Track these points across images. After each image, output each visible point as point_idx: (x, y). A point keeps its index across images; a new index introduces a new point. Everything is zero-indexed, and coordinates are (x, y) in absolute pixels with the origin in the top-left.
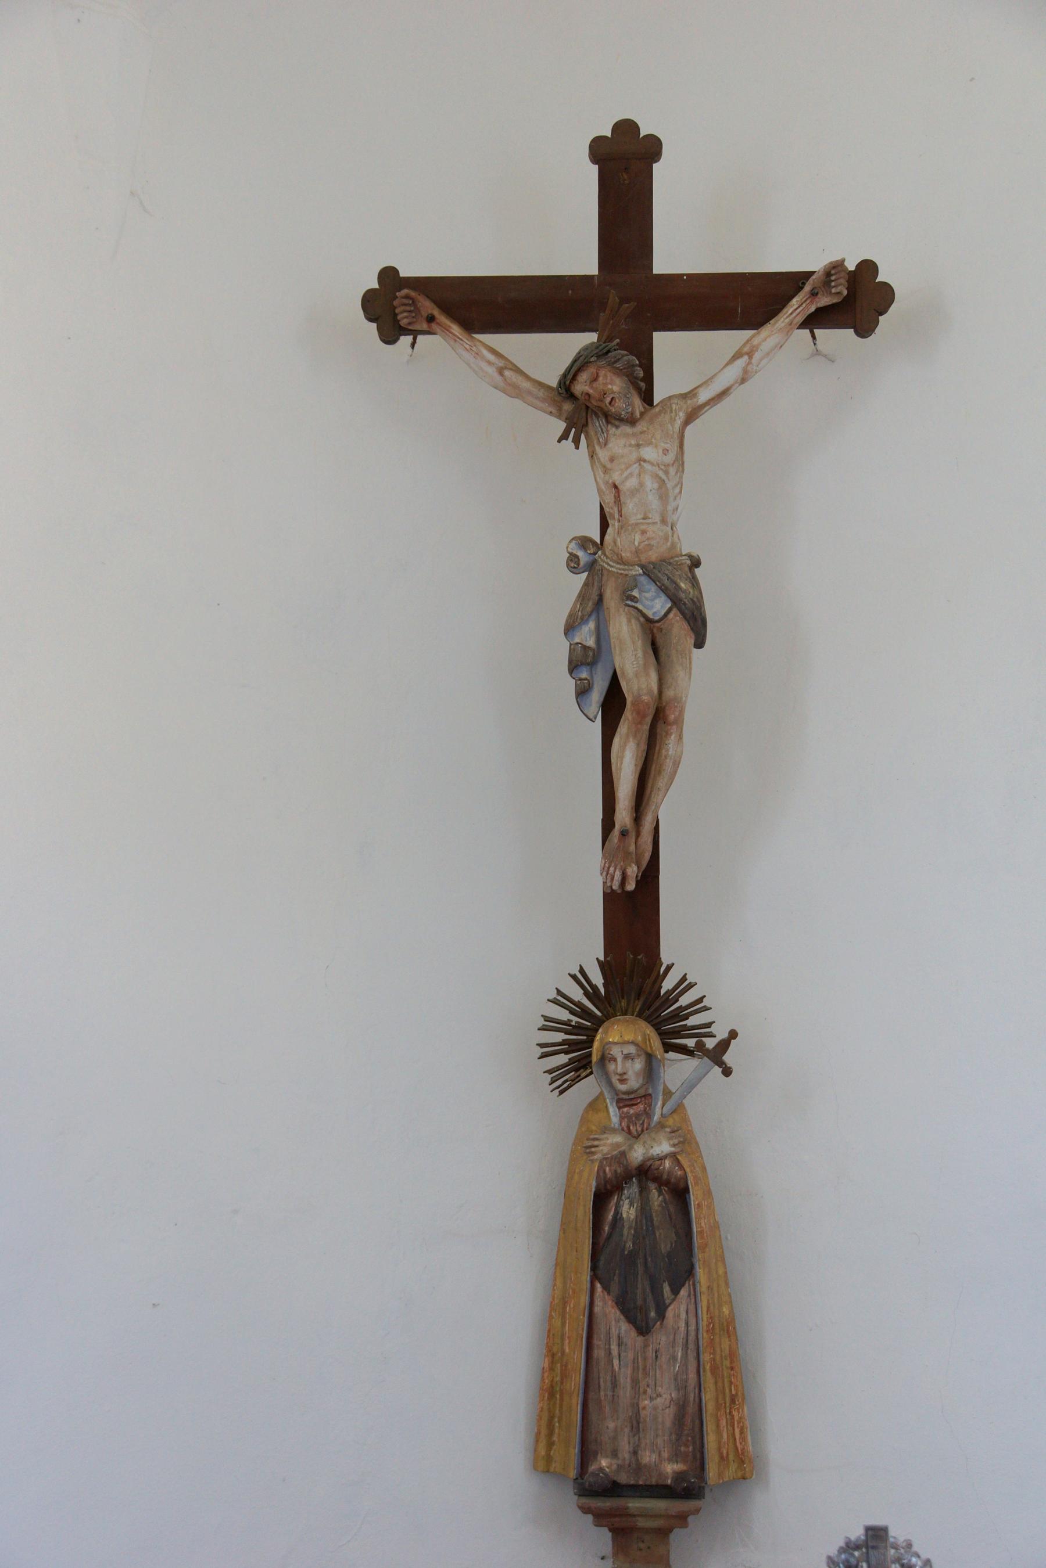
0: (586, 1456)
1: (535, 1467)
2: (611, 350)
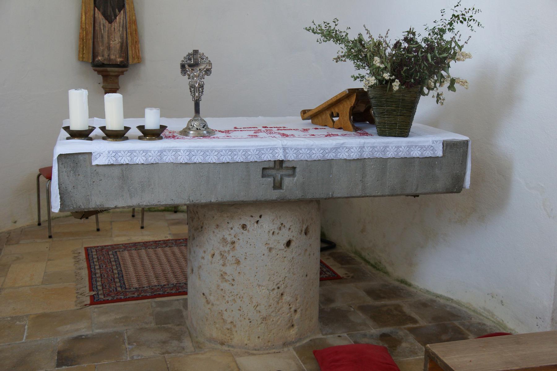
0: (94, 56)
1: (81, 59)
2: (324, 136)
